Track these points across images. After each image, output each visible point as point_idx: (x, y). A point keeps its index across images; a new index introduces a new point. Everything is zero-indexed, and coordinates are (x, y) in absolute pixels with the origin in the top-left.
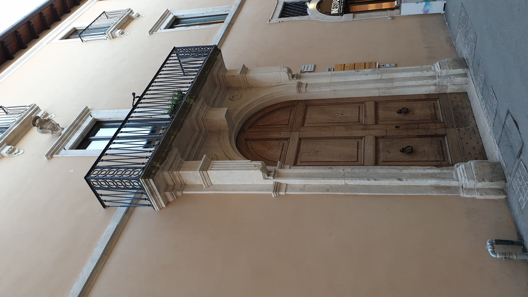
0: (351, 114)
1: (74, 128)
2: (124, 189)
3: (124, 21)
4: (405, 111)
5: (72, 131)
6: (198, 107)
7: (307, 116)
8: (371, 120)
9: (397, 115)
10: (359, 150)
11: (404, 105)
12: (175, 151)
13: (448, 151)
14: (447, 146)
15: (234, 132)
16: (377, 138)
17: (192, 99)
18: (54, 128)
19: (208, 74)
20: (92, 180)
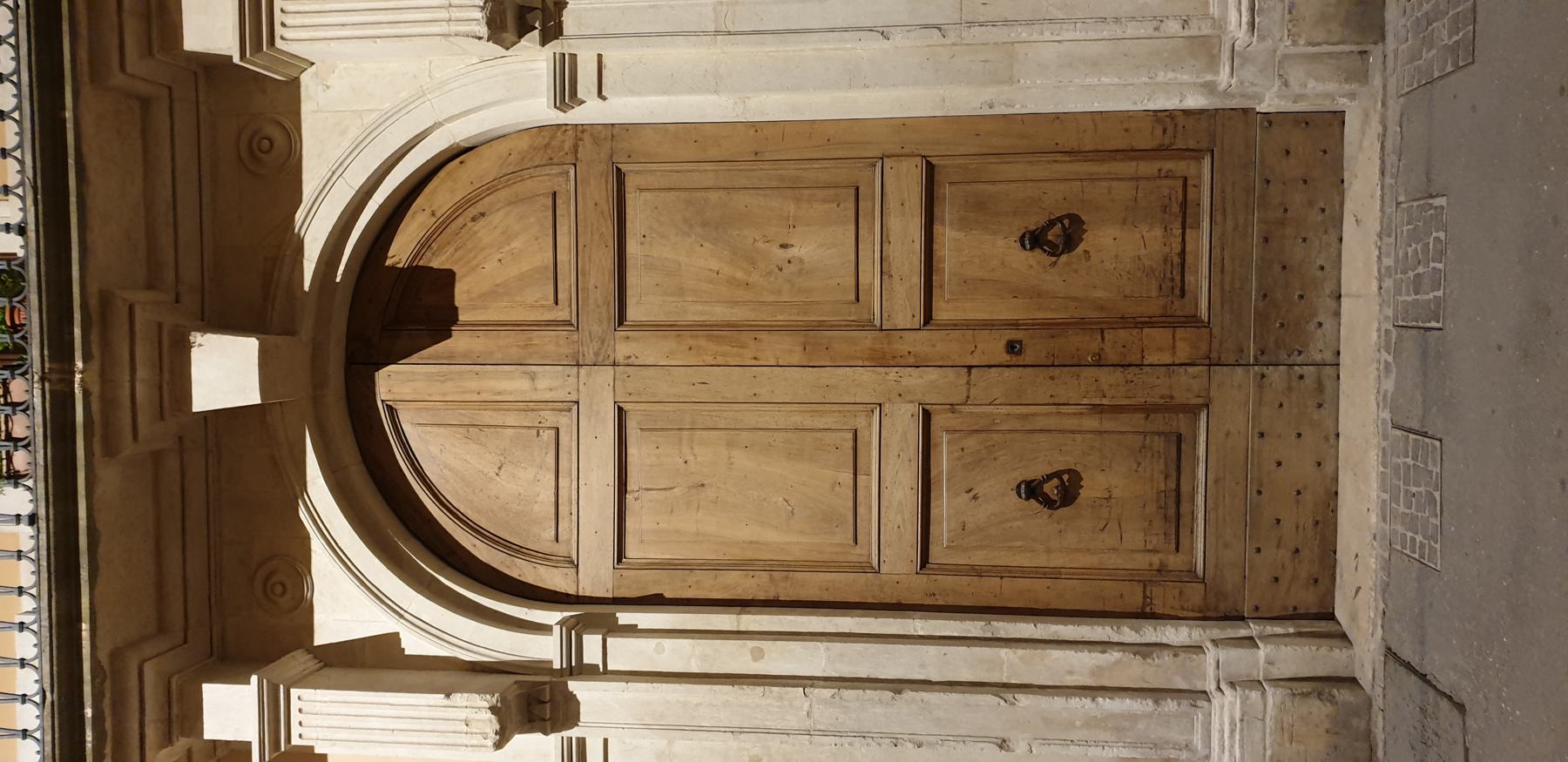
9: (1029, 263)
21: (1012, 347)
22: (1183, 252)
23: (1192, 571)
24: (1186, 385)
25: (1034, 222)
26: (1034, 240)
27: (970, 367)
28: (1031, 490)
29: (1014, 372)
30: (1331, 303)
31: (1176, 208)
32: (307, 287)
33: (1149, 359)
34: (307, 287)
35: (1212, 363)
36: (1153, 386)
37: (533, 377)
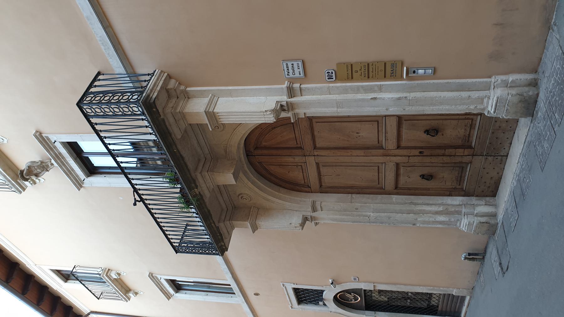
0: (367, 134)
1: (59, 159)
2: (129, 115)
3: (120, 287)
4: (432, 131)
5: (62, 162)
6: (203, 185)
7: (316, 133)
8: (391, 144)
9: (425, 136)
10: (380, 174)
11: (434, 126)
12: (221, 225)
13: (466, 178)
14: (467, 173)
15: (245, 165)
16: (397, 165)
17: (194, 189)
18: (43, 167)
19: (178, 150)
20: (85, 107)
21: (420, 152)
22: (469, 135)
23: (462, 189)
24: (466, 159)
25: (428, 128)
26: (427, 132)
27: (409, 156)
28: (423, 176)
29: (420, 158)
30: (509, 145)
31: (469, 126)
32: (211, 130)
33: (457, 154)
34: (211, 130)
35: (473, 155)
36: (458, 159)
37: (294, 158)
